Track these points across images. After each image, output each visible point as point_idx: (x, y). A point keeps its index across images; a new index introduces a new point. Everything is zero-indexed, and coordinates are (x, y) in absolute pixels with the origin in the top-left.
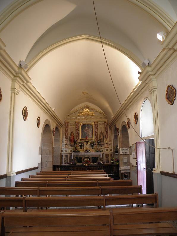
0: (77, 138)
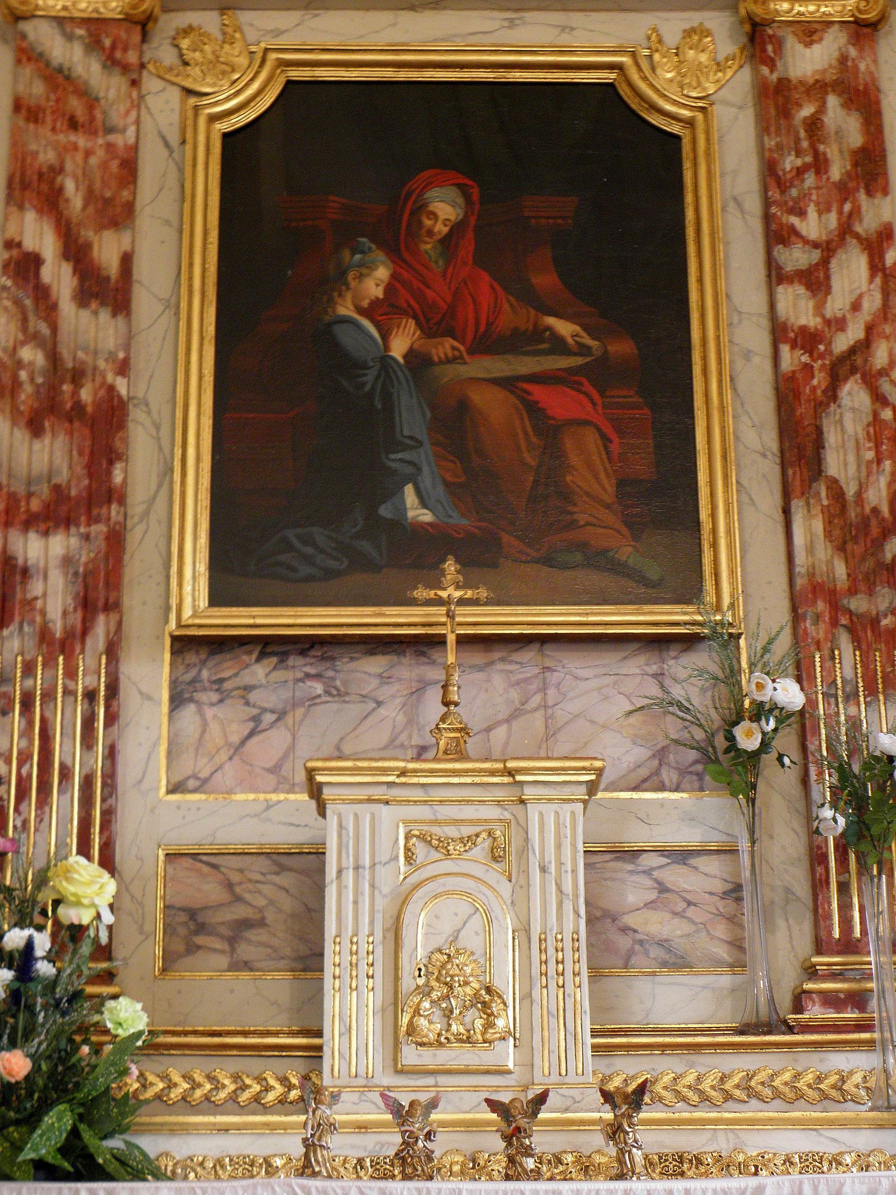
0: (54, 597)
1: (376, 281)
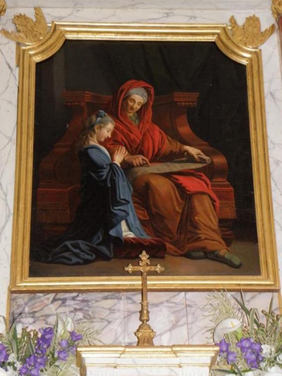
1: (107, 129)
